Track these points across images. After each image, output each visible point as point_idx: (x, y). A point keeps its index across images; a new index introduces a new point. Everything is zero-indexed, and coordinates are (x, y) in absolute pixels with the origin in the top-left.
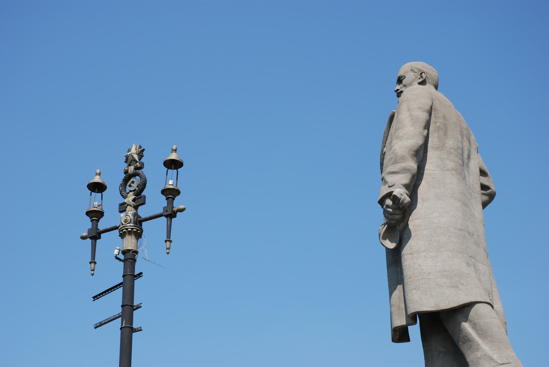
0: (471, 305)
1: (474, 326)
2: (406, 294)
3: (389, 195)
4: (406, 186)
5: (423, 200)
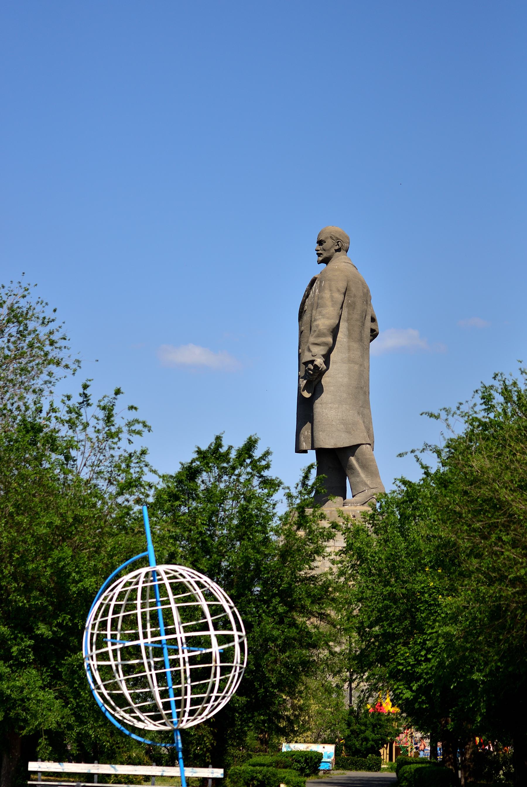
0: (358, 446)
1: (358, 460)
2: (314, 433)
3: (312, 362)
4: (324, 356)
5: (333, 363)
